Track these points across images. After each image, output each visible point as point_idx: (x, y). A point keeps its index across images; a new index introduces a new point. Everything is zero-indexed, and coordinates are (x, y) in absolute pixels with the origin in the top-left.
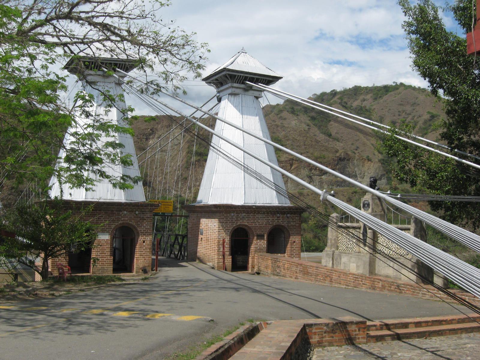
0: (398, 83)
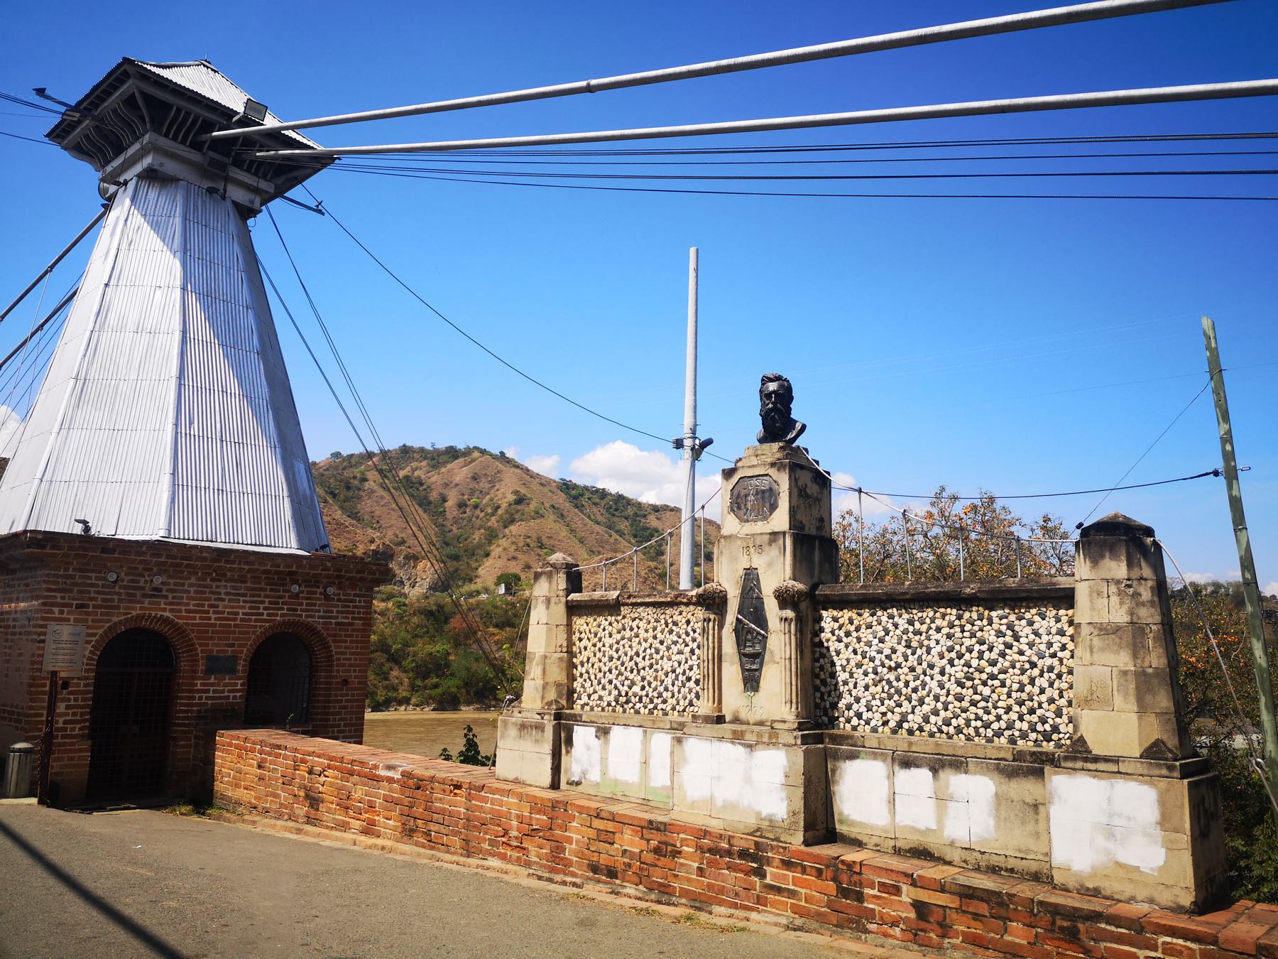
0: (471, 447)
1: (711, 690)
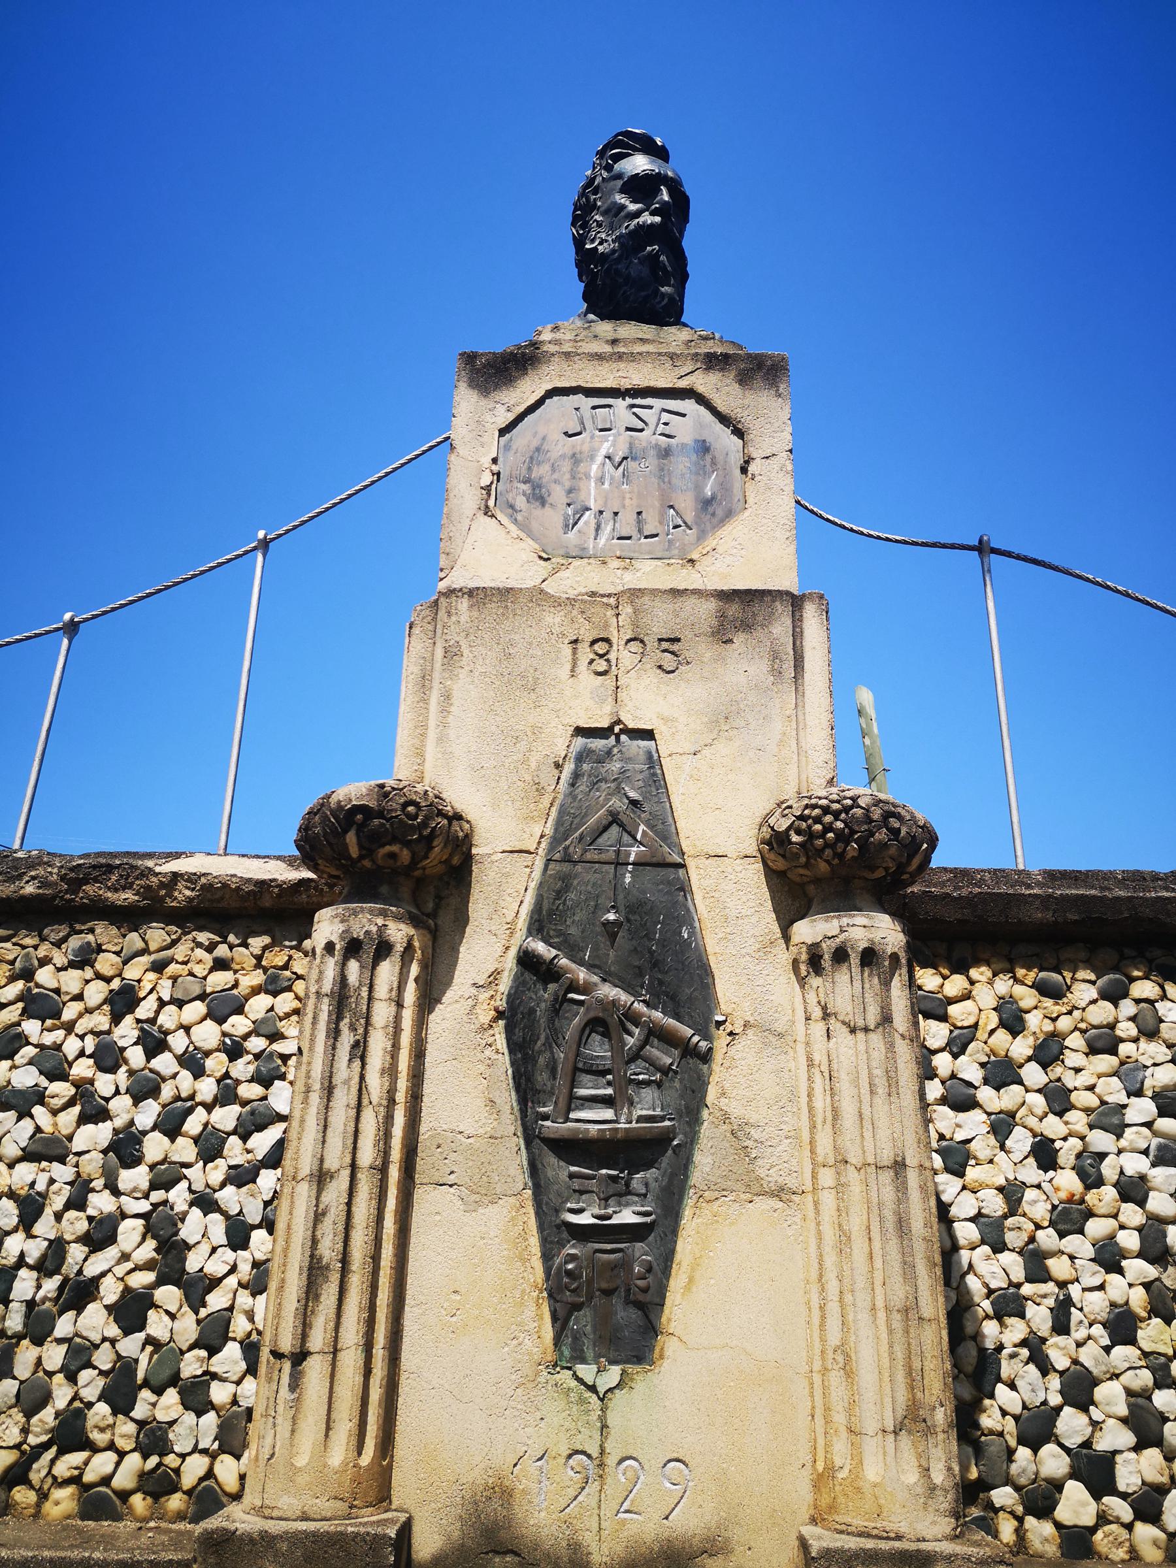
1: (351, 1360)
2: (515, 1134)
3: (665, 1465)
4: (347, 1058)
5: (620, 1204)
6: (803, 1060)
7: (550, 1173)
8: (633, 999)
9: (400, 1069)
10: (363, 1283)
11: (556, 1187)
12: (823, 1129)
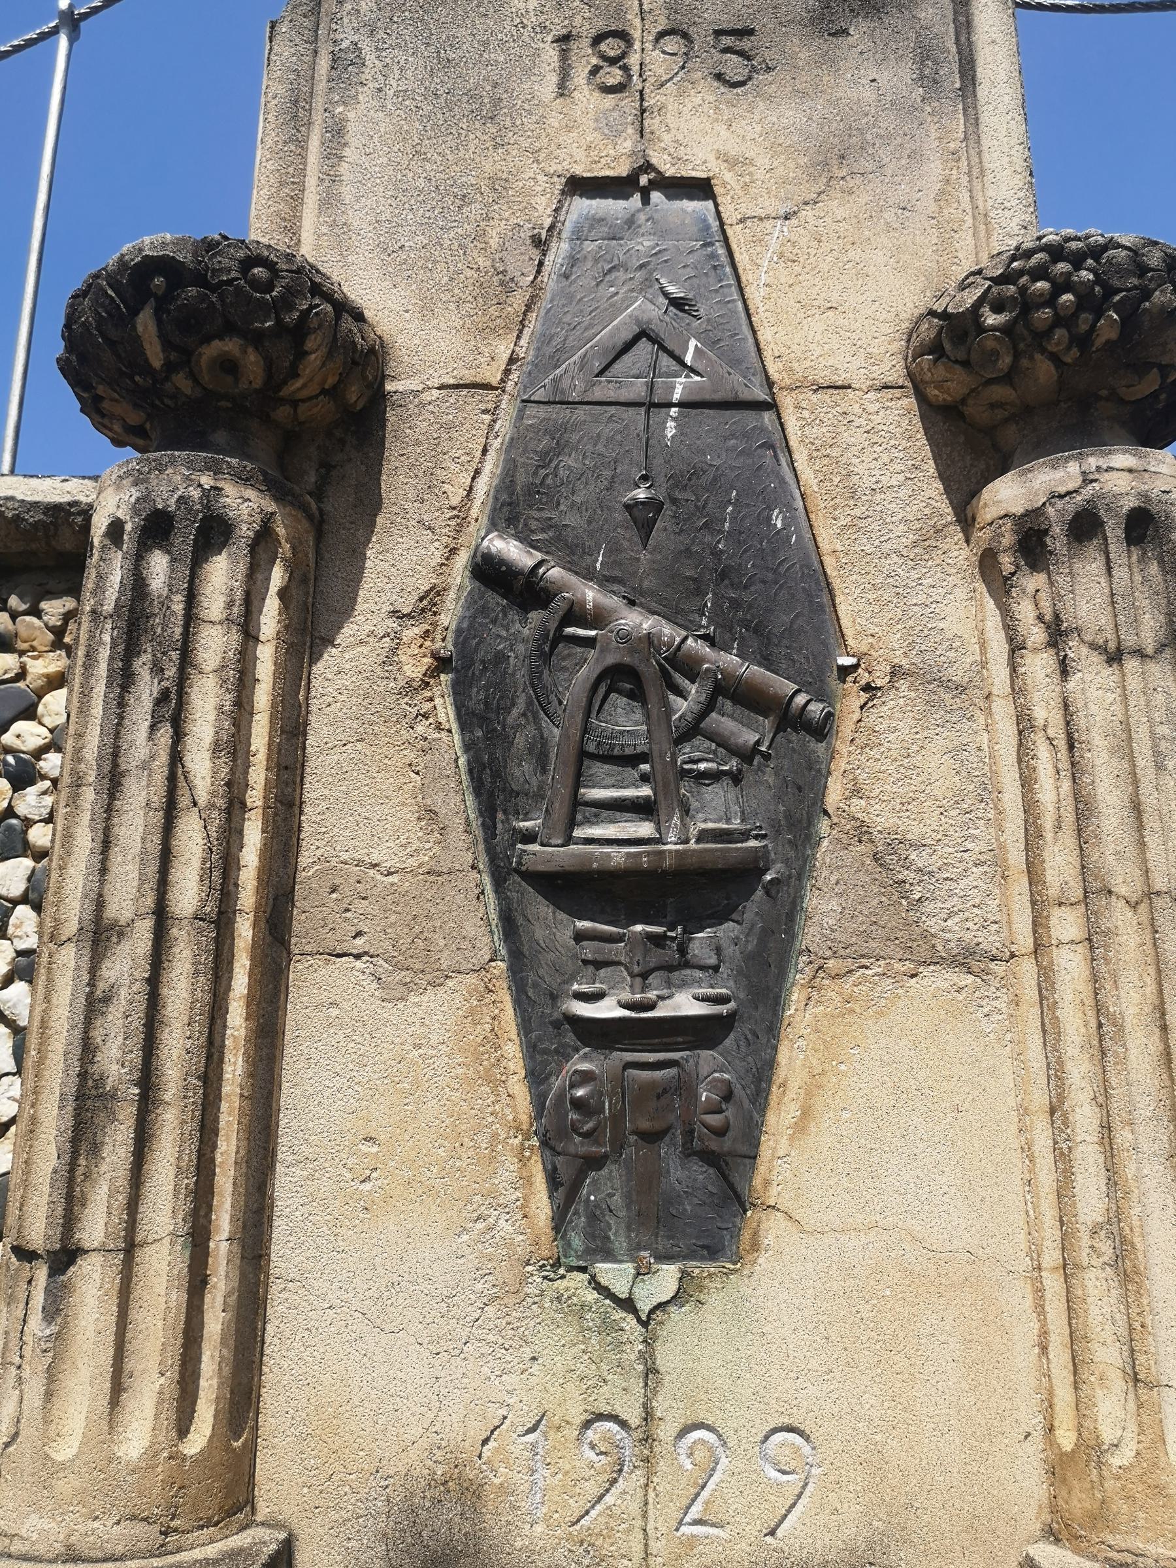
2: (473, 867)
3: (767, 1438)
4: (147, 724)
5: (669, 984)
6: (1007, 729)
7: (540, 933)
8: (684, 633)
9: (253, 748)
10: (184, 1122)
11: (551, 957)
12: (1056, 840)
